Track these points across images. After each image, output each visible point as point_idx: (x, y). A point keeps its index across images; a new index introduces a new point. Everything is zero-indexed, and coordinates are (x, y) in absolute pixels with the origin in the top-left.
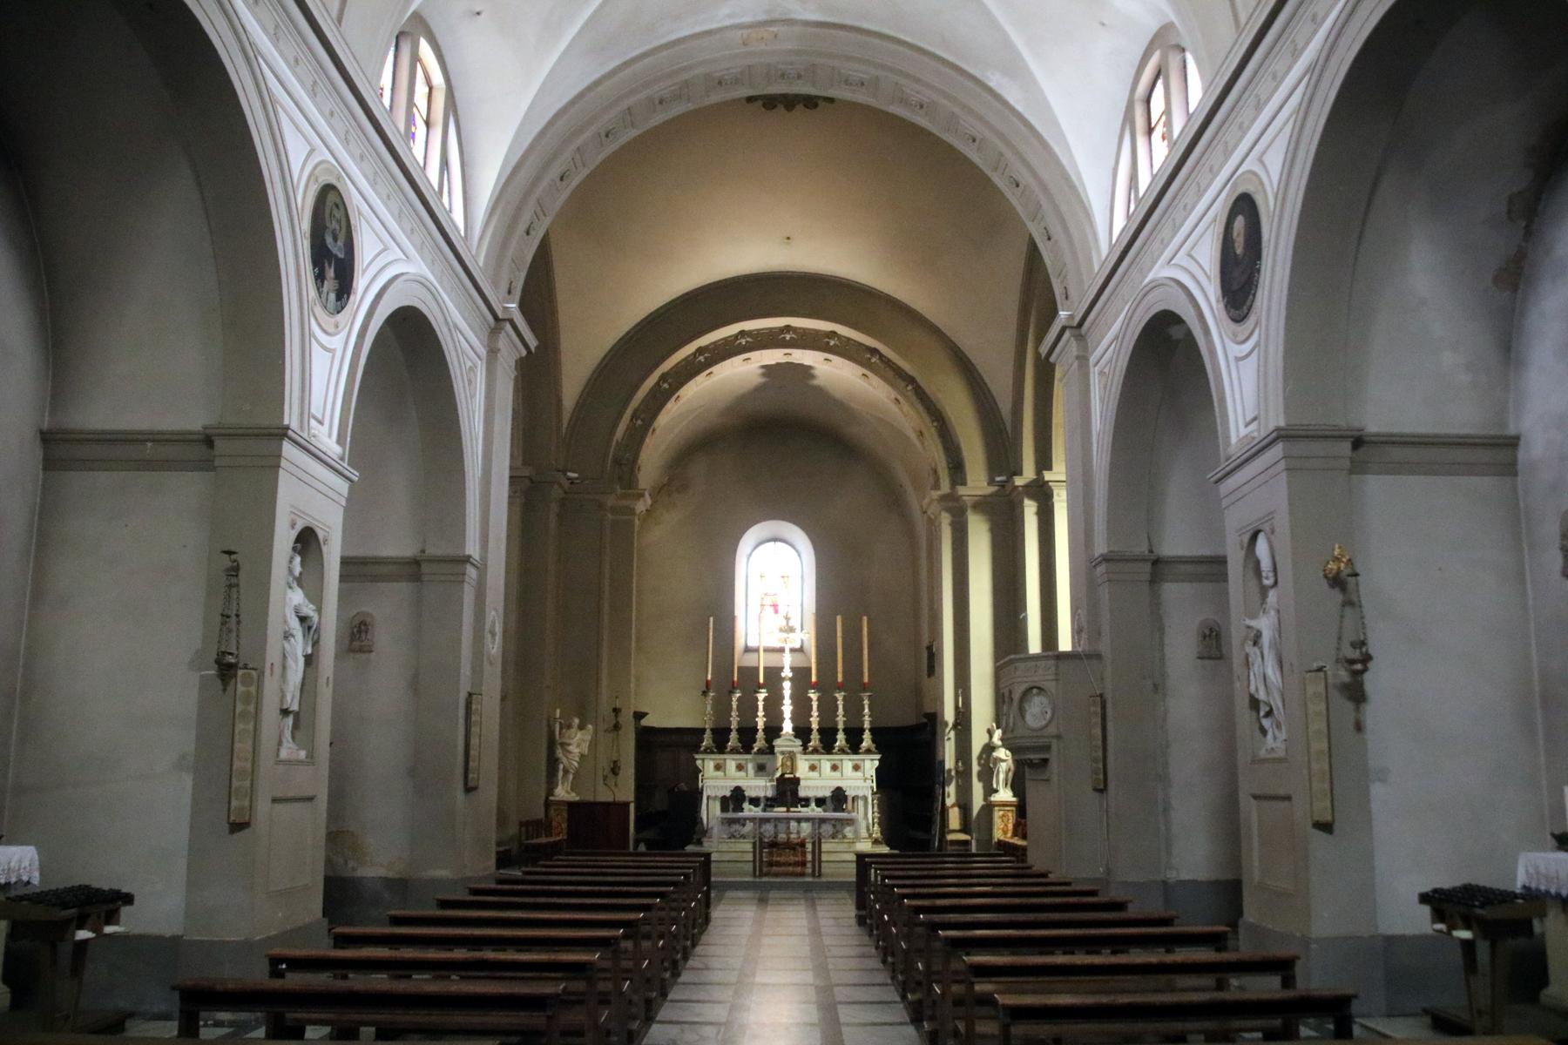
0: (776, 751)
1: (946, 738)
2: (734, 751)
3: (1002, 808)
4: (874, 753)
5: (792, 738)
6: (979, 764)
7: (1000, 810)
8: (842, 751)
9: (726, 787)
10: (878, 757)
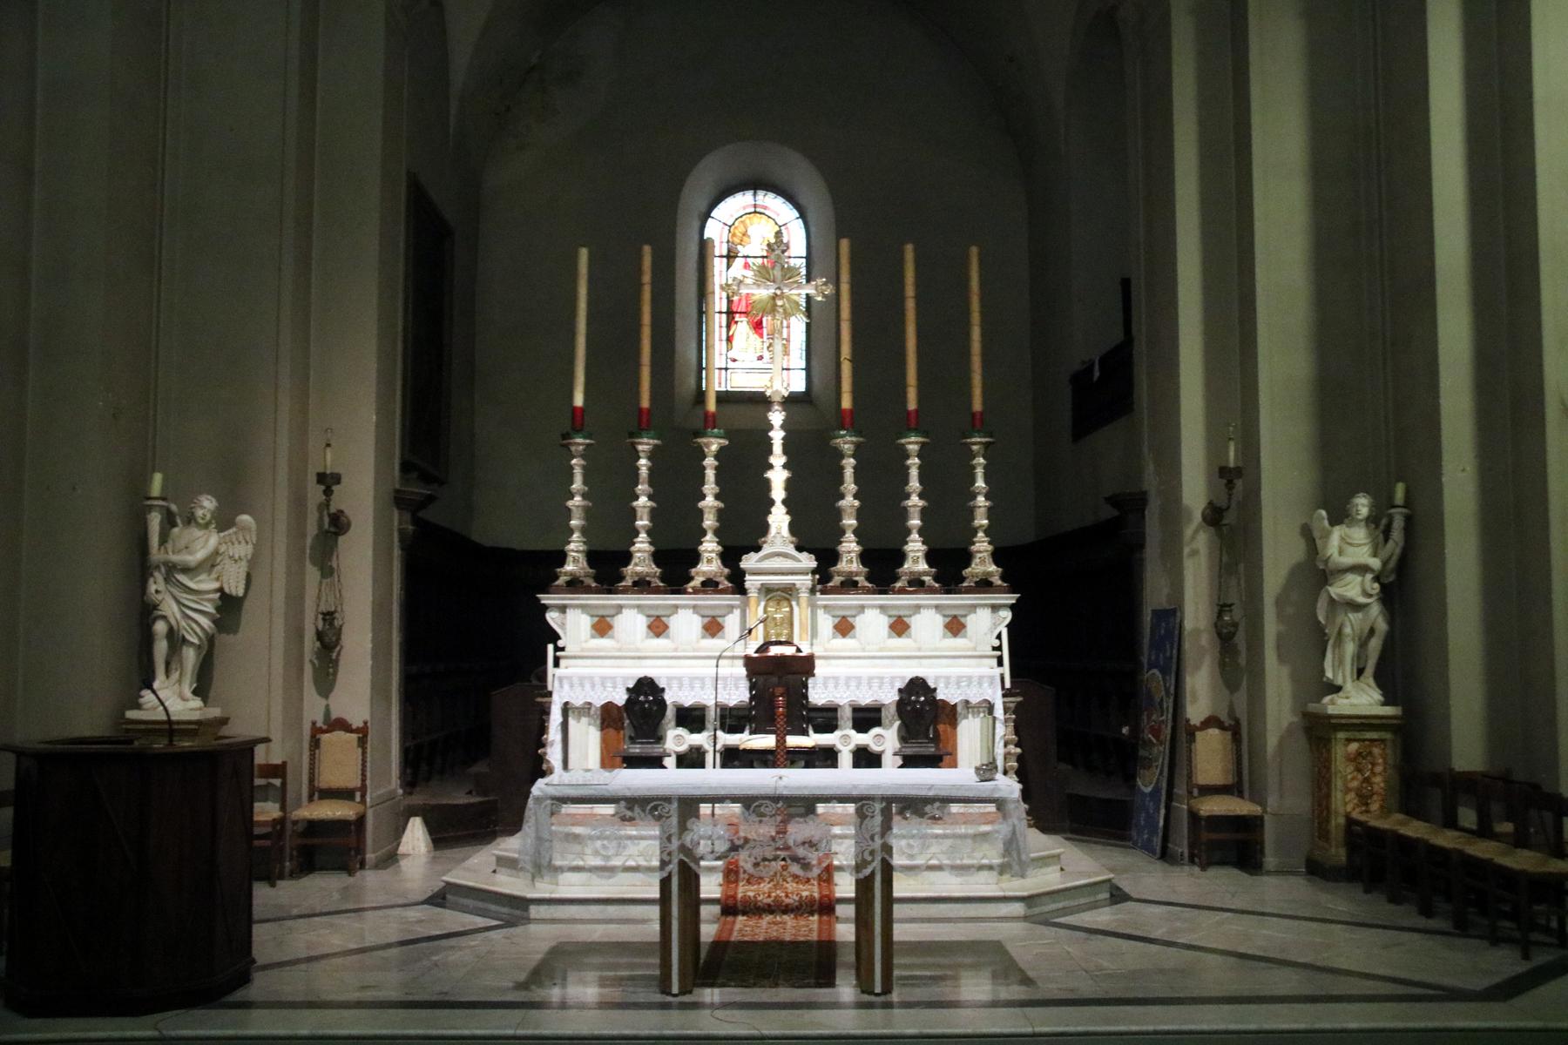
0: (747, 585)
1: (1186, 550)
2: (642, 585)
3: (1358, 735)
4: (999, 590)
5: (791, 550)
6: (1280, 616)
7: (1349, 741)
8: (917, 584)
9: (613, 679)
10: (1011, 599)
